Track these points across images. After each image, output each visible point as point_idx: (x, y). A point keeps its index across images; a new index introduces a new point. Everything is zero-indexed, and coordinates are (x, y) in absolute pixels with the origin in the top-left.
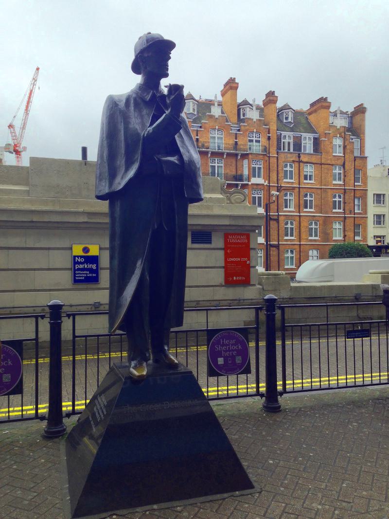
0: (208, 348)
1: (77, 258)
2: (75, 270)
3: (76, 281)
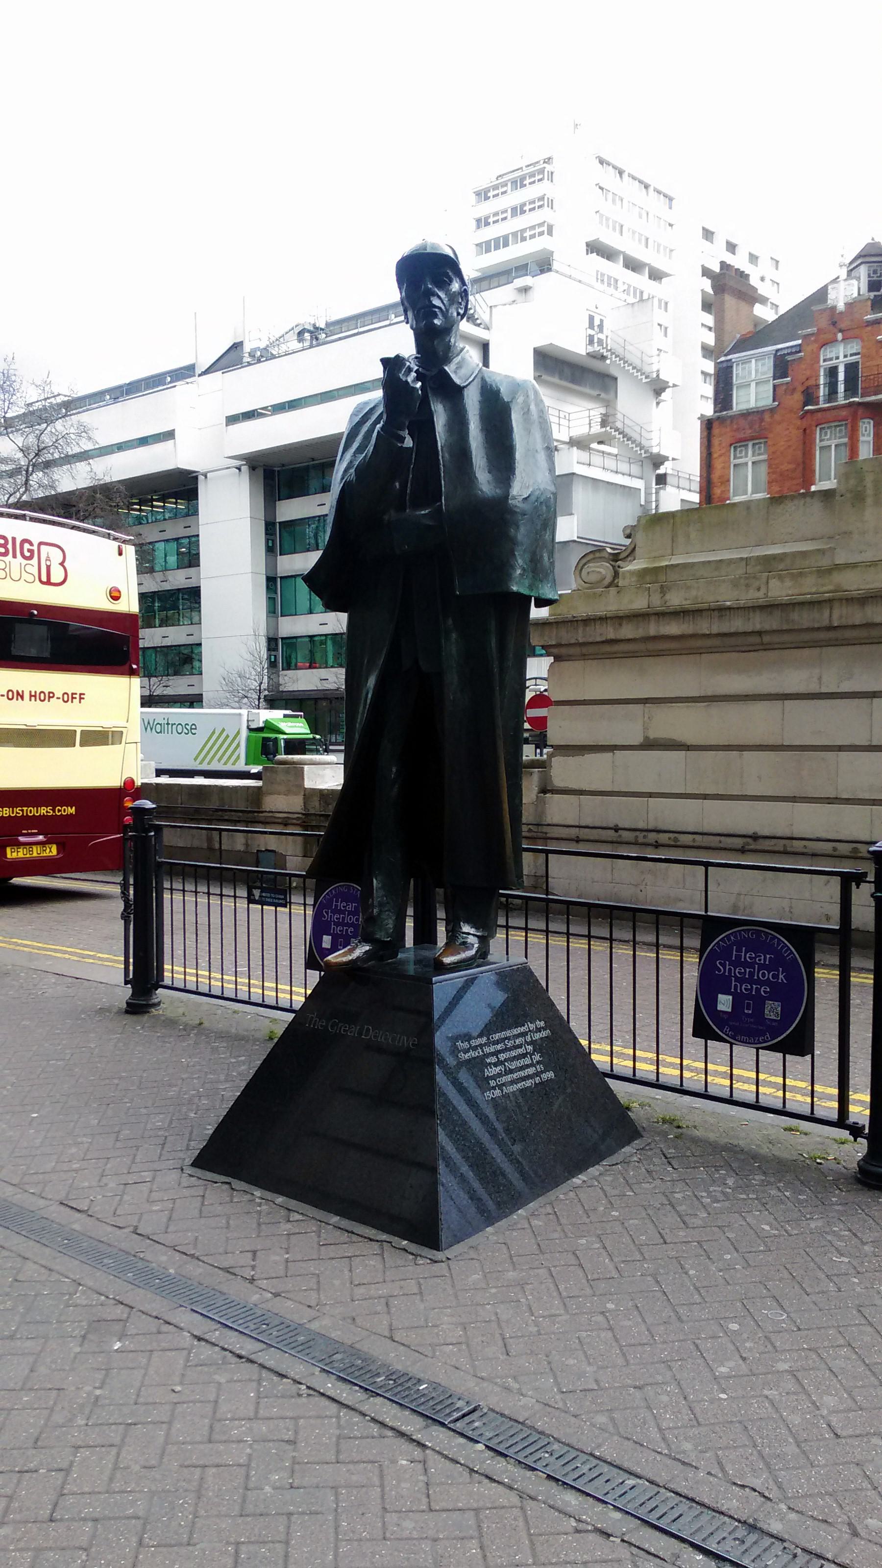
0: (700, 959)
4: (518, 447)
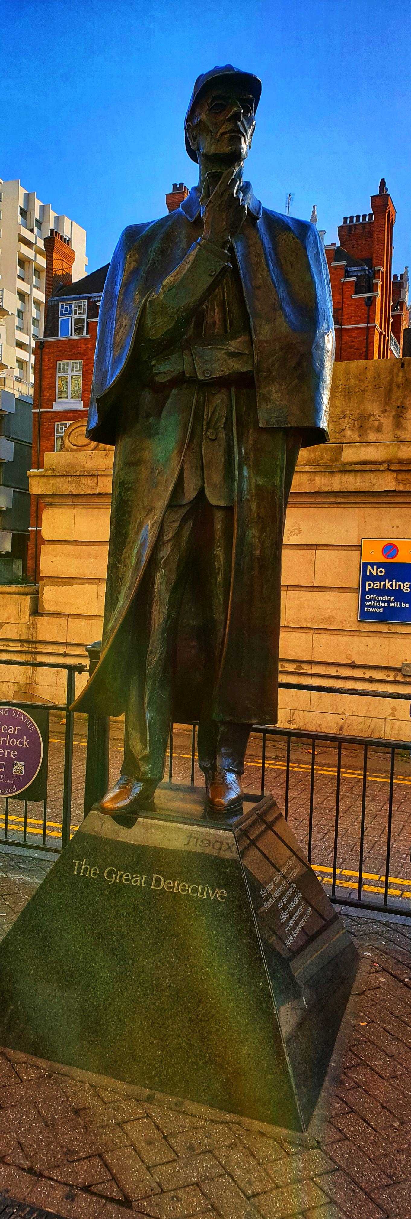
1: (369, 567)
2: (364, 593)
3: (365, 616)
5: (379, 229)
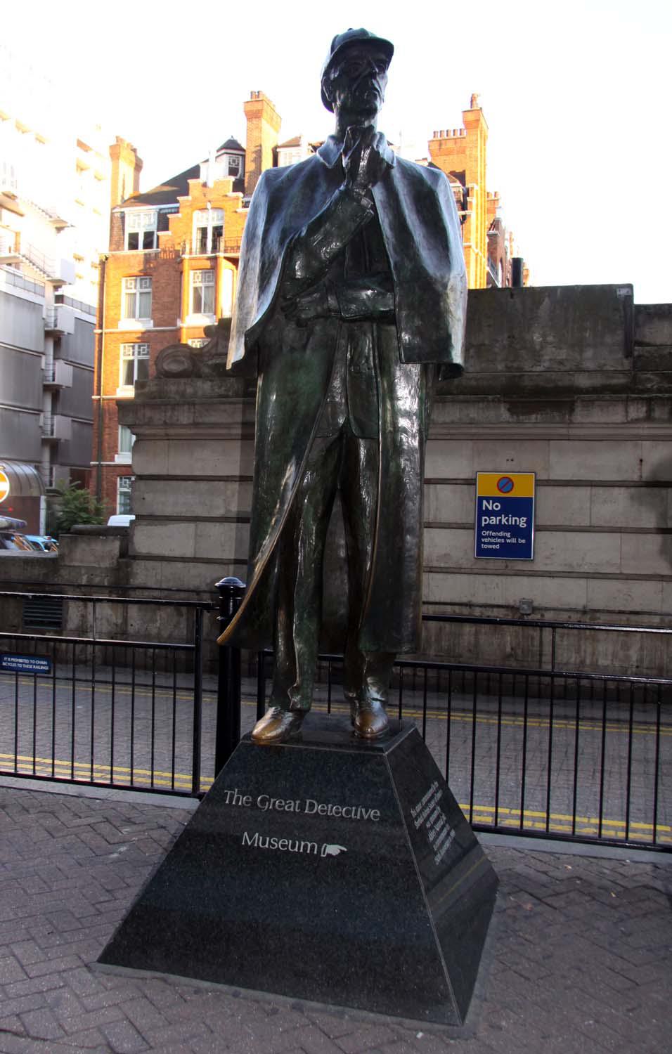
2: (480, 529)
3: (481, 552)
4: (256, 280)
5: (471, 145)
